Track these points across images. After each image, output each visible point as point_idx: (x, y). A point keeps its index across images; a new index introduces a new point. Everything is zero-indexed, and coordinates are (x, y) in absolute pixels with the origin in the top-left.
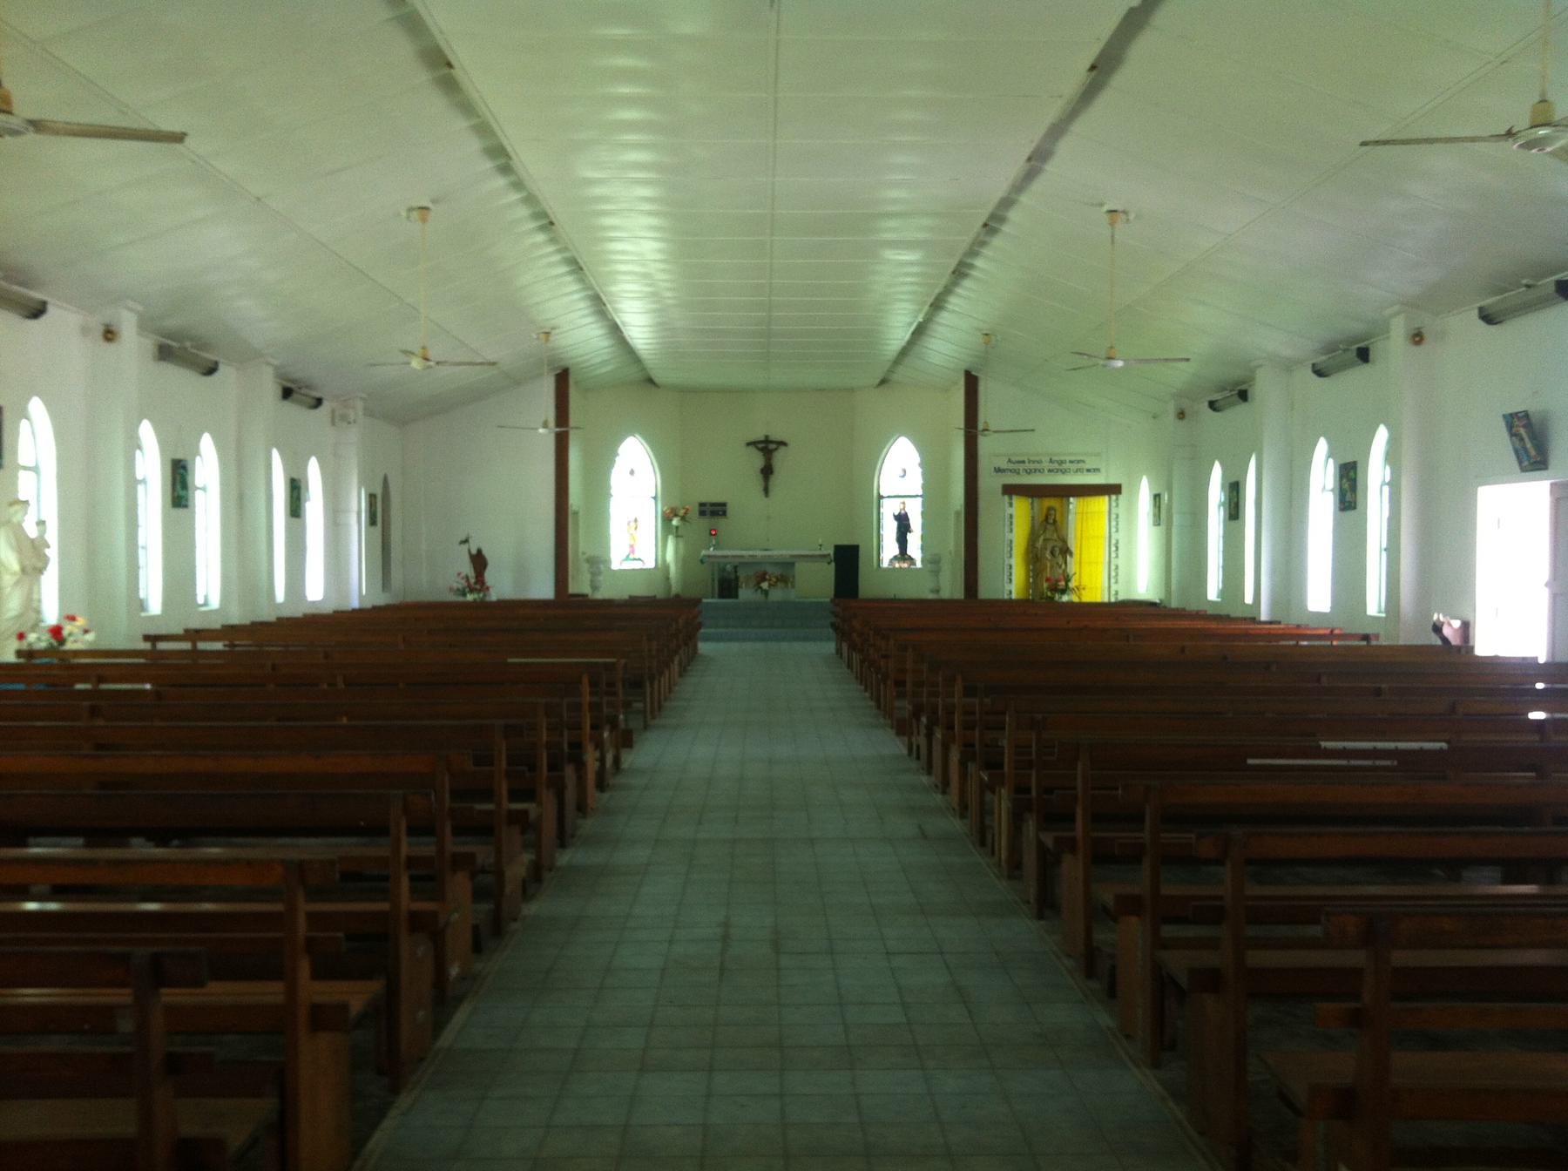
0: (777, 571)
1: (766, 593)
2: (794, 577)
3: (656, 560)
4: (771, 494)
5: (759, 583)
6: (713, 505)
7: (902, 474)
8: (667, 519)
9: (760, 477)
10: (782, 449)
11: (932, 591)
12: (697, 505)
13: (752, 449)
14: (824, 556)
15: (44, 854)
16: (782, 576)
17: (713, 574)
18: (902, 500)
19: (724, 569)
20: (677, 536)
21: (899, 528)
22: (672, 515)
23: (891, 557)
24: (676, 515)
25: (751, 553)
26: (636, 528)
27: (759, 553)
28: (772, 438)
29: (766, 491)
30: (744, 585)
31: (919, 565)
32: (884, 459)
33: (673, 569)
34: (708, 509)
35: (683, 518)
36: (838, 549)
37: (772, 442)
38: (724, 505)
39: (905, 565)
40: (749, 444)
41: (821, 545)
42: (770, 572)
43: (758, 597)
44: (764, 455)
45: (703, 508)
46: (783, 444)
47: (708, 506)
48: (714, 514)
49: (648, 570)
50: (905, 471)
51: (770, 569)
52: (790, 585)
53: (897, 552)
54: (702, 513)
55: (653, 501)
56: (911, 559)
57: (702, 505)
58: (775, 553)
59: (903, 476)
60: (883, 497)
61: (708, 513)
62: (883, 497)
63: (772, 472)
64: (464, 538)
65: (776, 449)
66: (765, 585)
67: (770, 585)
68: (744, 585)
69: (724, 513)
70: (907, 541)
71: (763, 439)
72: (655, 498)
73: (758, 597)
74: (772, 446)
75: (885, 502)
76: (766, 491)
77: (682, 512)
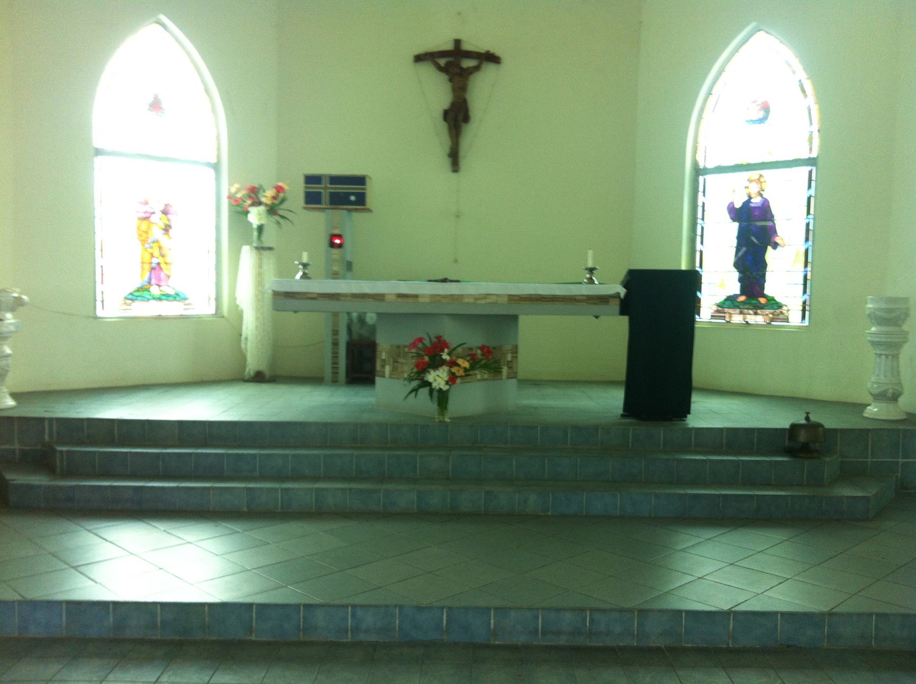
0: (474, 339)
1: (442, 398)
2: (515, 350)
3: (218, 299)
4: (464, 163)
5: (422, 369)
6: (336, 180)
7: (761, 114)
8: (239, 211)
9: (443, 127)
10: (489, 70)
11: (880, 397)
12: (301, 180)
13: (428, 72)
14: (603, 300)
15: (82, 481)
16: (487, 351)
17: (335, 333)
18: (754, 174)
19: (362, 320)
20: (260, 249)
21: (743, 238)
22: (249, 202)
23: (721, 298)
24: (257, 203)
25: (404, 288)
26: (167, 229)
27: (426, 289)
28: (466, 47)
29: (454, 158)
30: (387, 369)
31: (795, 319)
32: (702, 109)
33: (250, 324)
34: (325, 190)
35: (272, 210)
36: (439, 338)
37: (469, 55)
38: (360, 180)
39: (757, 319)
40: (419, 58)
41: (591, 270)
42: (453, 343)
43: (423, 403)
44: (451, 80)
45: (315, 188)
46: (491, 58)
47: (325, 183)
48: (338, 200)
49: (197, 320)
50: (766, 108)
51: (454, 334)
52: (505, 370)
53: (734, 288)
54: (312, 199)
55: (212, 172)
56: (774, 304)
57: (311, 180)
58: (469, 289)
59: (762, 120)
60: (706, 171)
61: (325, 197)
62: (706, 171)
63: (466, 119)
64: (597, 315)
65: (477, 68)
66: (438, 378)
67: (452, 379)
68: (387, 369)
69: (361, 199)
70: (764, 265)
71: (449, 46)
72: (216, 167)
73: (423, 403)
74: (468, 63)
75: (711, 181)
76: (454, 158)
77: (267, 196)
